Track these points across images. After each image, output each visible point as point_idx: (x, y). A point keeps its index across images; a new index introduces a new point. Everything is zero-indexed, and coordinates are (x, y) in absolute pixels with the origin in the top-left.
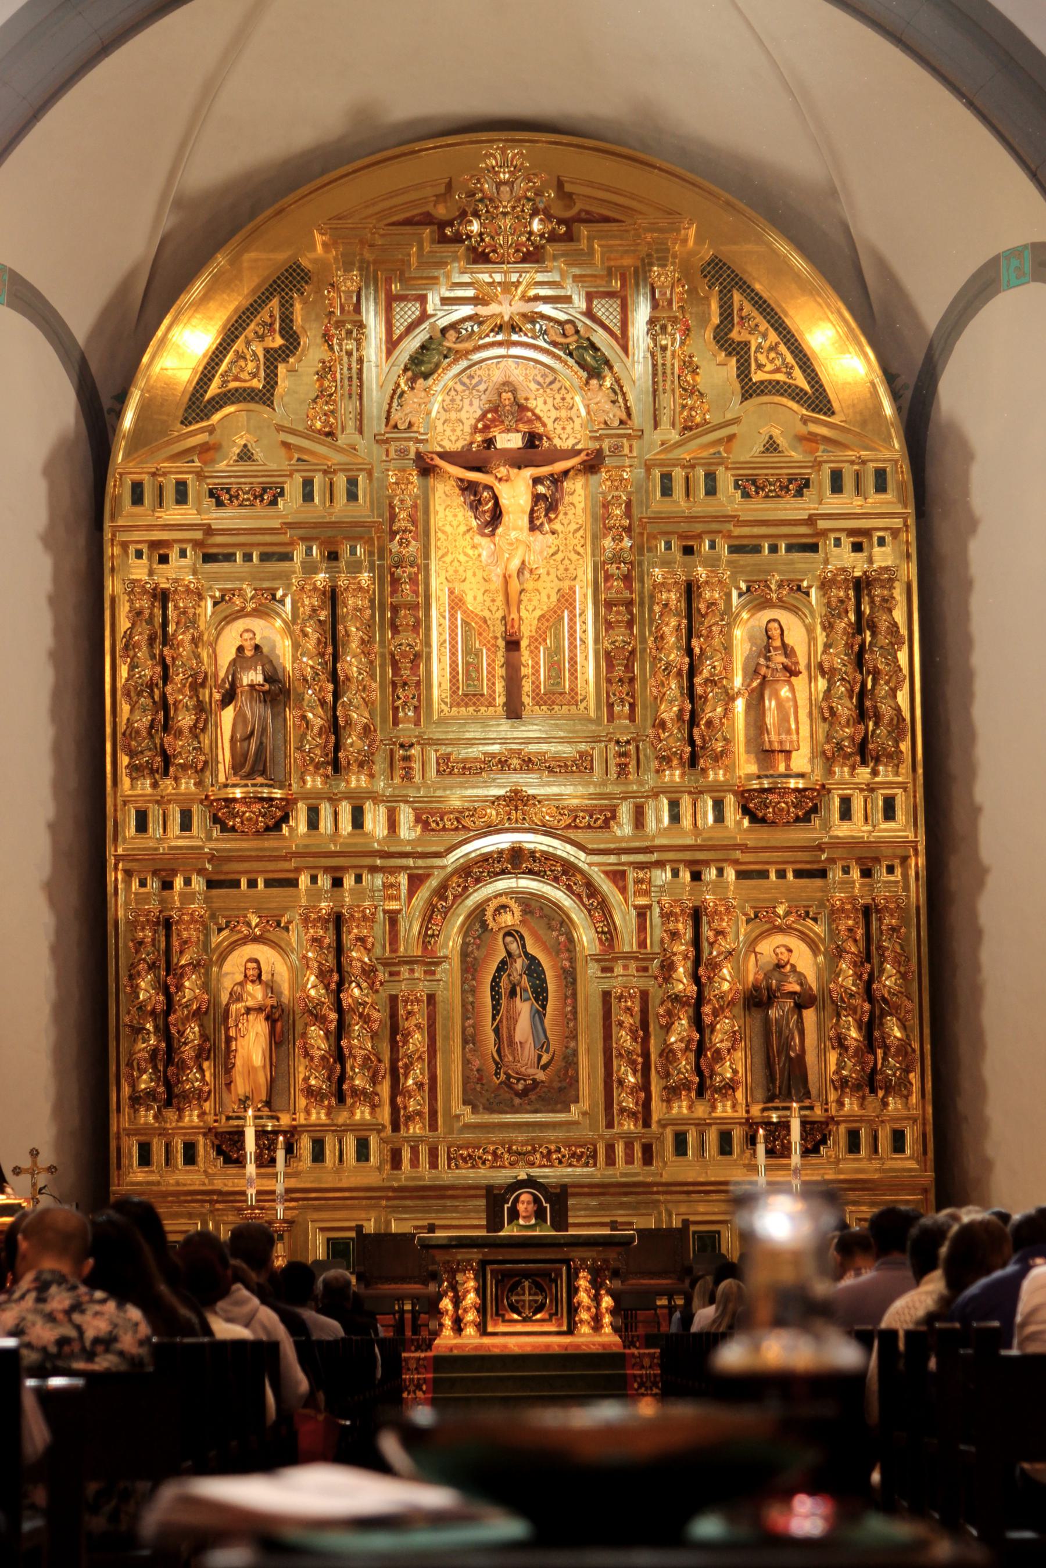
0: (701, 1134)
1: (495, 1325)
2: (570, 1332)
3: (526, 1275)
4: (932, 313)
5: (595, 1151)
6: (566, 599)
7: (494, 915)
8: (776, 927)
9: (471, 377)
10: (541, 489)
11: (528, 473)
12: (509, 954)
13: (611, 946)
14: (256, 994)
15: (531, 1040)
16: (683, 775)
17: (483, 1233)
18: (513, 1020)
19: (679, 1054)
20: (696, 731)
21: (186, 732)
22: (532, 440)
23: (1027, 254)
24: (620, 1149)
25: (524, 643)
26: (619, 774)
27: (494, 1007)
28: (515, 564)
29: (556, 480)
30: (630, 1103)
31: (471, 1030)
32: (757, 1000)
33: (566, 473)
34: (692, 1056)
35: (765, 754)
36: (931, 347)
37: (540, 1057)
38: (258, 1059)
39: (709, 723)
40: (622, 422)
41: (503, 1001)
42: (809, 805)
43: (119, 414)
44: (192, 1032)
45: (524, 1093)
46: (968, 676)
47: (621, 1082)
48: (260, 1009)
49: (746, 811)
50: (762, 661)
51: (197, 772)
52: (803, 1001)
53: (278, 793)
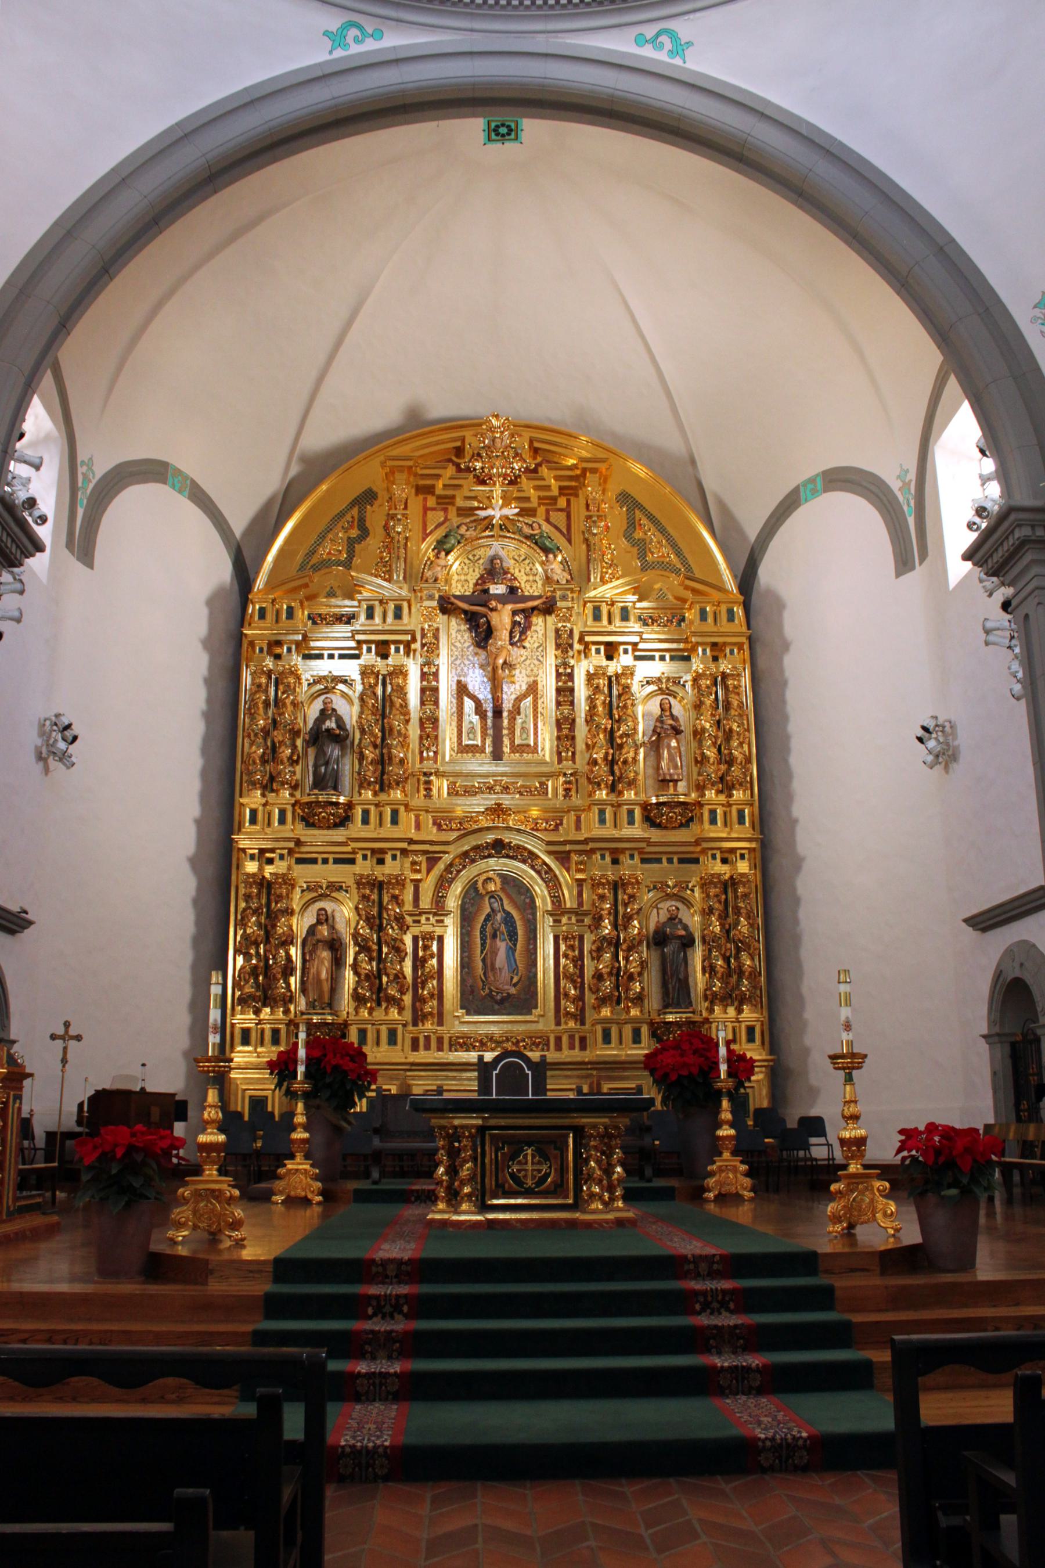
5: (548, 1040)
6: (533, 689)
7: (483, 884)
8: (667, 895)
9: (474, 556)
10: (517, 618)
12: (493, 910)
13: (560, 905)
15: (506, 967)
16: (607, 795)
17: (474, 1096)
18: (495, 952)
19: (606, 976)
20: (616, 767)
21: (285, 760)
22: (513, 590)
23: (819, 480)
24: (565, 1039)
25: (505, 714)
26: (565, 796)
27: (482, 945)
29: (528, 613)
30: (572, 1009)
31: (466, 959)
32: (659, 939)
33: (533, 609)
34: (613, 979)
35: (664, 782)
37: (512, 978)
39: (625, 762)
40: (567, 581)
41: (488, 941)
42: (687, 814)
45: (503, 1001)
46: (786, 738)
47: (566, 995)
50: (658, 724)
51: (291, 787)
53: (342, 800)
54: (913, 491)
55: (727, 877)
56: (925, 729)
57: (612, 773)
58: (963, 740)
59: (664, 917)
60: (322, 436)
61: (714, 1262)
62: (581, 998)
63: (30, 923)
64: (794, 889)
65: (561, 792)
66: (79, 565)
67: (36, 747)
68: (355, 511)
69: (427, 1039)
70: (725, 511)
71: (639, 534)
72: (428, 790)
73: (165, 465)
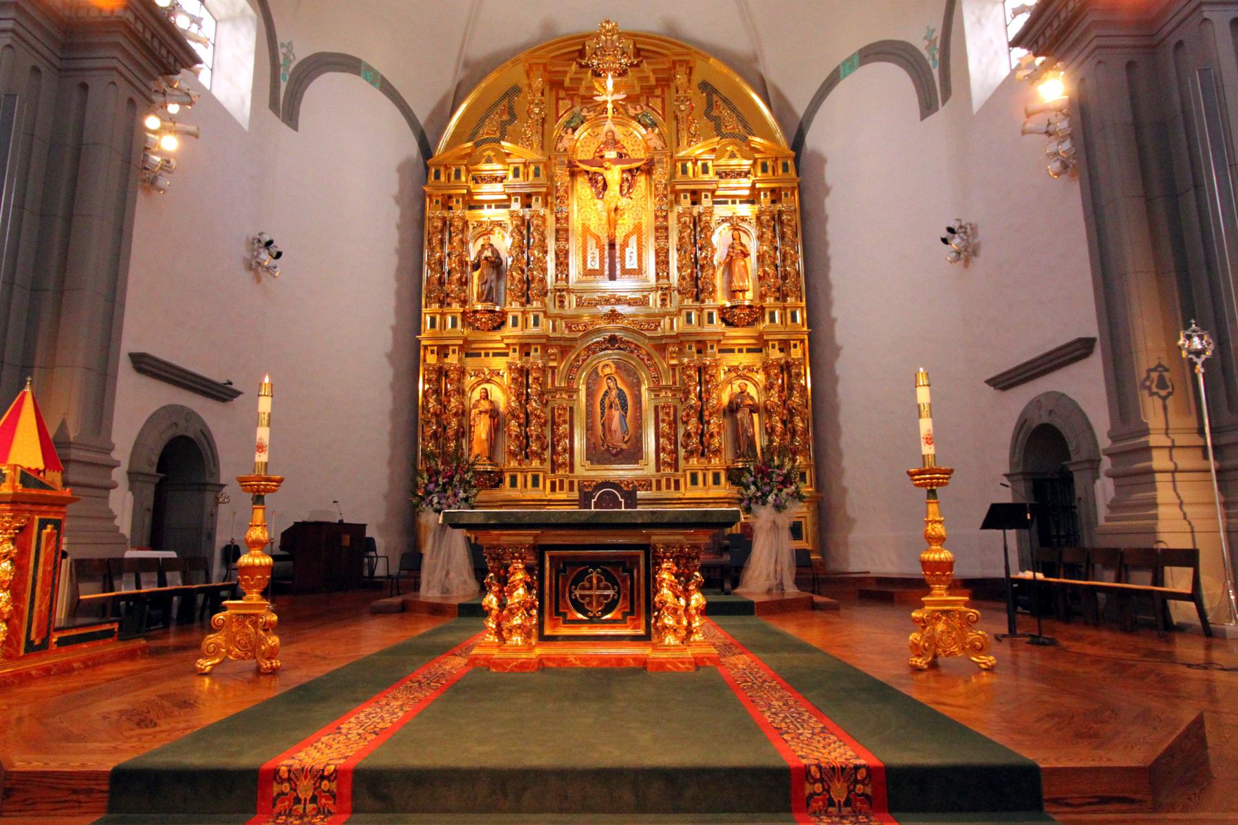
0: (704, 475)
1: (555, 626)
2: (646, 638)
3: (595, 563)
4: (800, 110)
11: (619, 167)
14: (485, 405)
18: (611, 419)
22: (620, 155)
24: (664, 483)
25: (618, 247)
28: (613, 206)
32: (732, 409)
33: (637, 169)
35: (732, 293)
36: (801, 124)
38: (484, 436)
43: (437, 143)
44: (454, 423)
47: (664, 450)
48: (486, 412)
49: (724, 320)
52: (754, 409)
53: (498, 309)
54: (938, 45)
55: (783, 361)
56: (951, 230)
57: (697, 286)
58: (983, 235)
59: (737, 389)
60: (480, 49)
61: (856, 782)
62: (676, 451)
63: (238, 393)
64: (833, 370)
65: (659, 302)
66: (284, 126)
67: (245, 259)
68: (505, 102)
69: (562, 482)
70: (781, 96)
71: (715, 113)
72: (562, 302)
73: (359, 61)
